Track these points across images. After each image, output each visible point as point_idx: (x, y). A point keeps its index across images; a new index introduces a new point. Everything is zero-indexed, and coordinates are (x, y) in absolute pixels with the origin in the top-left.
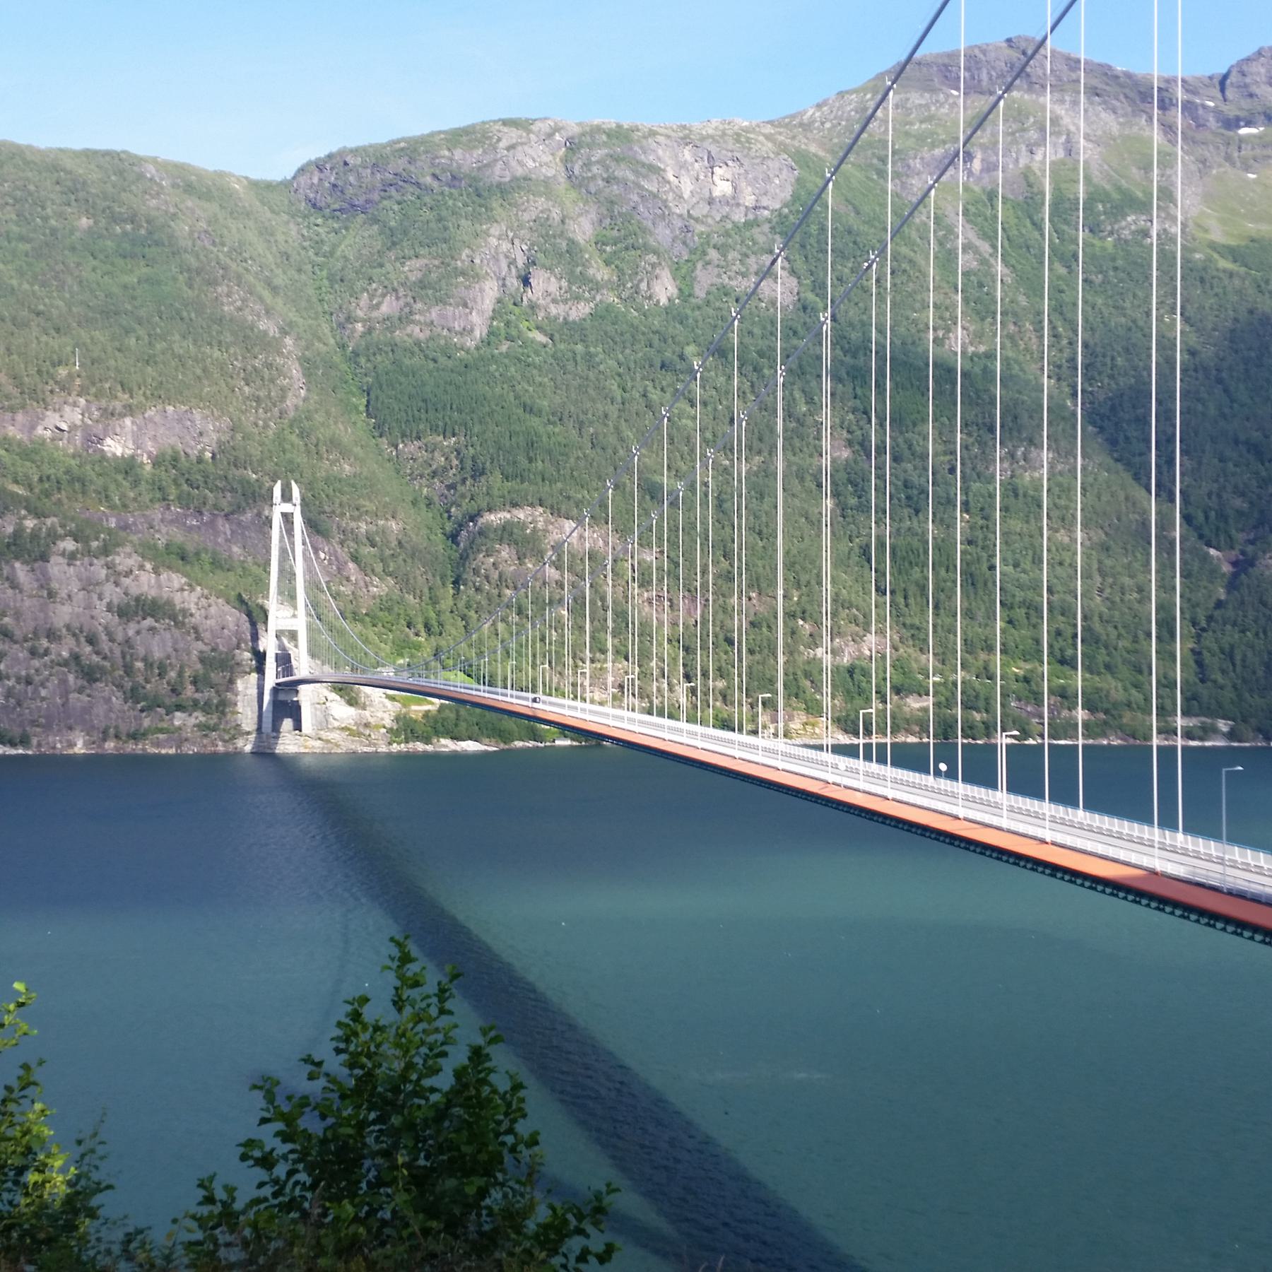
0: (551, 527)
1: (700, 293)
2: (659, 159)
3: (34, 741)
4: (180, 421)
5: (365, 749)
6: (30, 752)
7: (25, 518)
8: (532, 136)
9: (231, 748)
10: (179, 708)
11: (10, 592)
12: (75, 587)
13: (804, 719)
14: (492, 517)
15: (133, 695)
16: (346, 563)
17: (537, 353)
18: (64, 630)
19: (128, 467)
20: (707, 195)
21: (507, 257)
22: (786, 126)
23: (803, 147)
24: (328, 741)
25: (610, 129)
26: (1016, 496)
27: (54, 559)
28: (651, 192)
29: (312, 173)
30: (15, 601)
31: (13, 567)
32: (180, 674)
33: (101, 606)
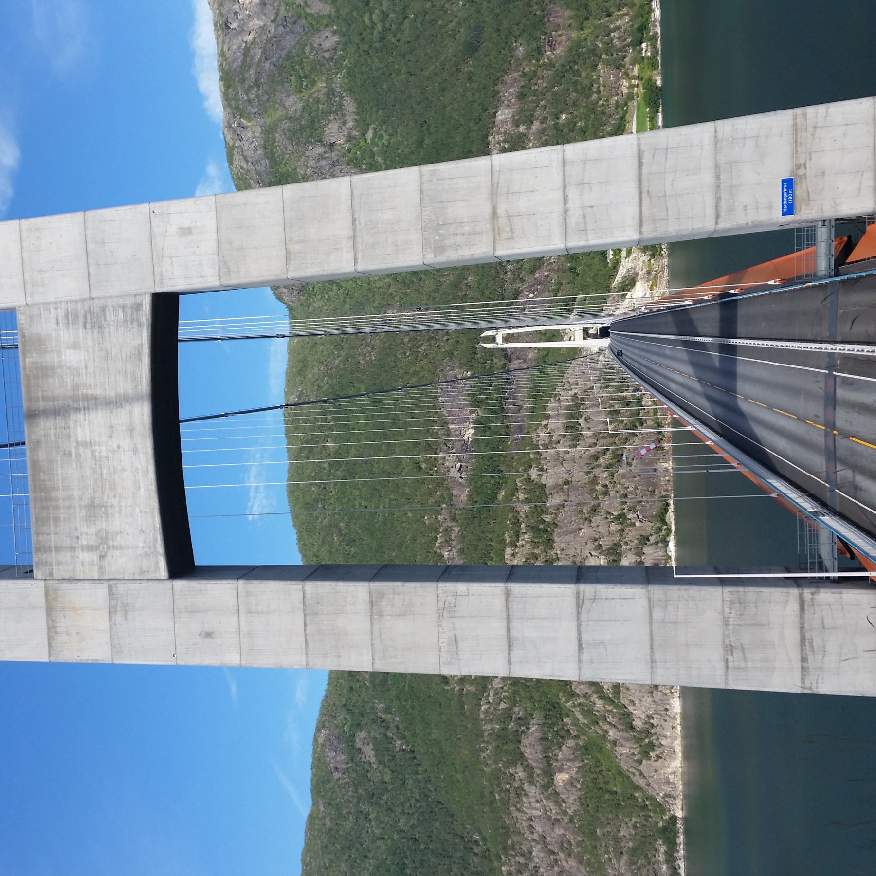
0: (502, 130)
2: (239, 48)
3: (664, 493)
5: (666, 274)
7: (518, 498)
8: (236, 145)
16: (535, 279)
17: (381, 137)
19: (481, 426)
20: (109, 424)
21: (318, 160)
25: (224, 85)
27: (543, 480)
28: (263, 53)
29: (281, 293)
31: (551, 507)
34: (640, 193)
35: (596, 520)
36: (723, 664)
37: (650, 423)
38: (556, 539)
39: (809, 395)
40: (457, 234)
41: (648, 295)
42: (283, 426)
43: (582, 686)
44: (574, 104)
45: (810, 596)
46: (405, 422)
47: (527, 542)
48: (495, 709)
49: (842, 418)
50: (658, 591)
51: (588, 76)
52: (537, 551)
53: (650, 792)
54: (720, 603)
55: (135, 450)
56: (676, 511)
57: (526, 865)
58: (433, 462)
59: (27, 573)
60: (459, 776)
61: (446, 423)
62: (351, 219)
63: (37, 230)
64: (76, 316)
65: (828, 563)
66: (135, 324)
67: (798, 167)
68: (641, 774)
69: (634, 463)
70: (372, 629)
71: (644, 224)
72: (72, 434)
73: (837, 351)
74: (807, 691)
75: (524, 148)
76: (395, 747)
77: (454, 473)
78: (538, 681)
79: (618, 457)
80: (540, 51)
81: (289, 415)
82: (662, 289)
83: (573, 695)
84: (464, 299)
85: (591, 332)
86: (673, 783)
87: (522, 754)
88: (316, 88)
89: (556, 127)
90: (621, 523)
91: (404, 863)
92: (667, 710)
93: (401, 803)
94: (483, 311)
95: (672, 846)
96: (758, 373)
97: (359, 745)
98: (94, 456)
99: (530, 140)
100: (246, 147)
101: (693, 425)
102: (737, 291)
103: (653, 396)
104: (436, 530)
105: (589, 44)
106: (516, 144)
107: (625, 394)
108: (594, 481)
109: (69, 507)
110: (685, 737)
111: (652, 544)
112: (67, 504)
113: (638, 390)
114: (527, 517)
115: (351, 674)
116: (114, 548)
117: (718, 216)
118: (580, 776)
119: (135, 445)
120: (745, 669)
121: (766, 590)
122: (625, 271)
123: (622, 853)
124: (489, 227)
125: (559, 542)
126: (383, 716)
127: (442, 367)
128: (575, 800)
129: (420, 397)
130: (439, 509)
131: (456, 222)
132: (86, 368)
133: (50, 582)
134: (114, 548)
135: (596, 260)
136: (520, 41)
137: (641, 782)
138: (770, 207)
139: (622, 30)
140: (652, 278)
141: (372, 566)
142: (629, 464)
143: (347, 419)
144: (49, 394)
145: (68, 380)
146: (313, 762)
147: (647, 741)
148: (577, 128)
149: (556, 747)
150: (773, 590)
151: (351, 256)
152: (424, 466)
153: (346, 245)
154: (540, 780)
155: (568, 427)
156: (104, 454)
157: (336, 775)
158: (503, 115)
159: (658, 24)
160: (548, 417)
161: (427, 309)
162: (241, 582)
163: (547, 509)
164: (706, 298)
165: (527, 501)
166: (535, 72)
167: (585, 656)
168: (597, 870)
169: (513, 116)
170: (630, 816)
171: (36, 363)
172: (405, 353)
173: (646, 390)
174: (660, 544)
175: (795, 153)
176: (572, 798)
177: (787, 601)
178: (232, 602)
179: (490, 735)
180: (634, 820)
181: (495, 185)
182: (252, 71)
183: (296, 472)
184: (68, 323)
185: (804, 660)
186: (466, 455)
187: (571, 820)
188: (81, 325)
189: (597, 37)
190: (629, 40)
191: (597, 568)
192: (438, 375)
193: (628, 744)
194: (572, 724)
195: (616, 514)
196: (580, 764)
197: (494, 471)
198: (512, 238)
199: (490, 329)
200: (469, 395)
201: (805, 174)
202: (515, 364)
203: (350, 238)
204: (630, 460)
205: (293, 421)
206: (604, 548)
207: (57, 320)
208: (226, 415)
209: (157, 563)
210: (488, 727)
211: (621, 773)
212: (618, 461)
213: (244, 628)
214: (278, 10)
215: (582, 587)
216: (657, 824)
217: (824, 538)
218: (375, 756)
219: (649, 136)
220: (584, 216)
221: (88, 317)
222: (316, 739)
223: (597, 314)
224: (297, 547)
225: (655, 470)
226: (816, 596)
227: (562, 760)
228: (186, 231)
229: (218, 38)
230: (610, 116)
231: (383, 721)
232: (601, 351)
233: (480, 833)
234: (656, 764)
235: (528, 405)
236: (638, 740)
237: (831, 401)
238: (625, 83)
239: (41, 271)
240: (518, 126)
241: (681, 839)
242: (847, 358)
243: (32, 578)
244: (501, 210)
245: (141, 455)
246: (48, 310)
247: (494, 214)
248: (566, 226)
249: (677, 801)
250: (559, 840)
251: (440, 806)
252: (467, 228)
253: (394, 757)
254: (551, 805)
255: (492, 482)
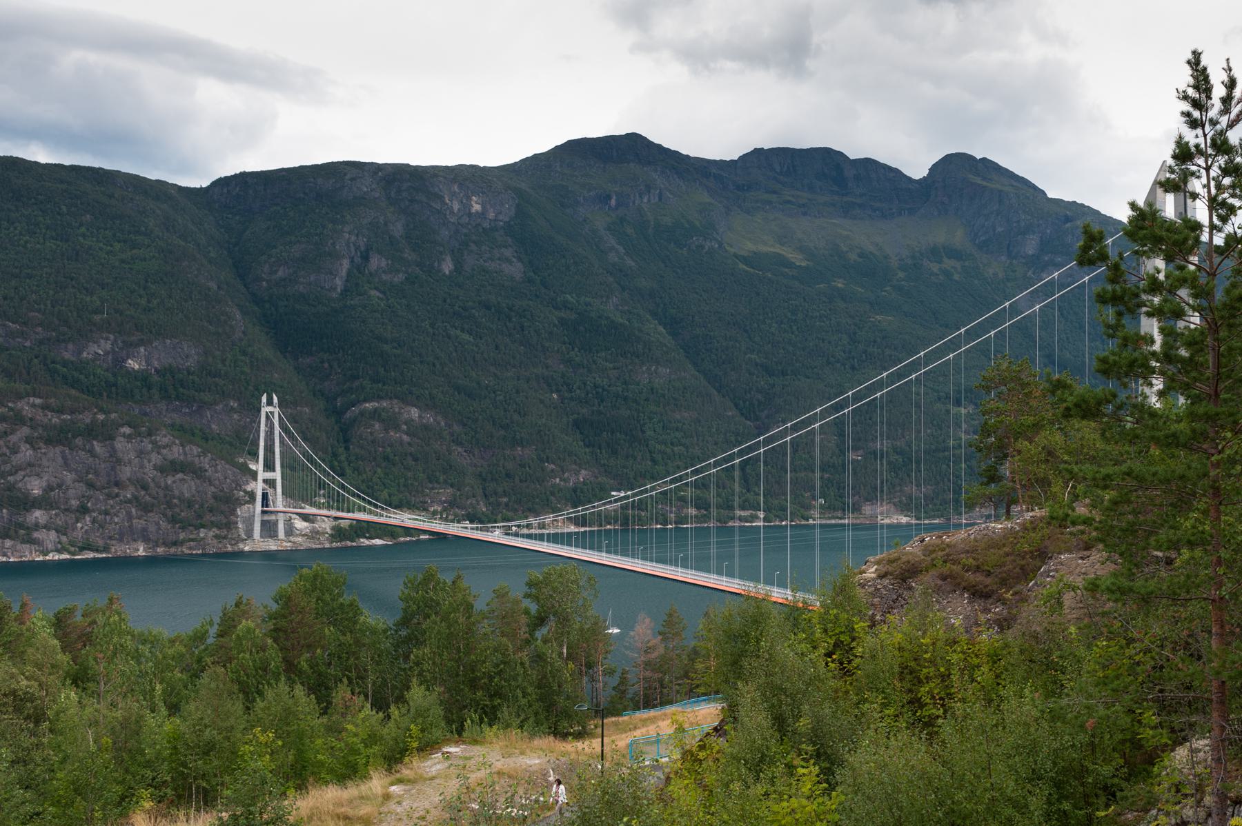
2: (440, 191)
4: (174, 348)
5: (317, 546)
6: (110, 556)
8: (366, 173)
9: (236, 548)
10: (203, 526)
12: (132, 455)
14: (367, 405)
15: (173, 520)
19: (143, 378)
24: (294, 543)
26: (653, 393)
30: (95, 464)
31: (93, 445)
32: (202, 506)
33: (149, 467)
35: (82, 487)
47: (50, 420)
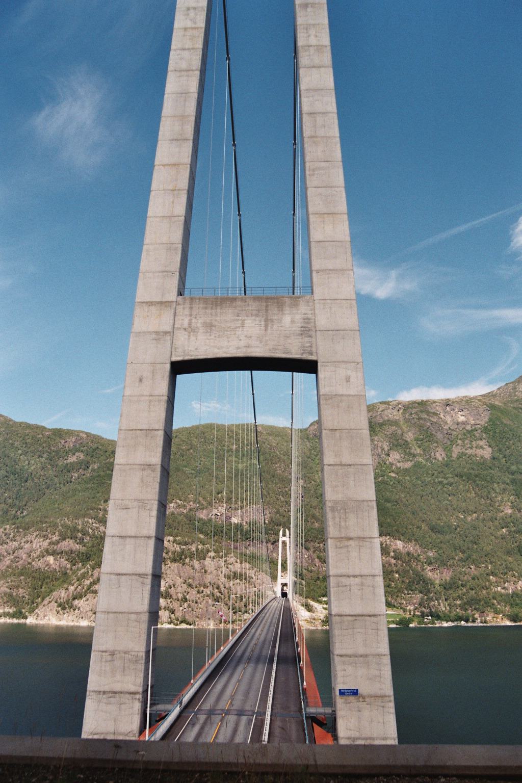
0: (392, 544)
1: (455, 455)
3: (196, 623)
5: (313, 628)
8: (390, 407)
11: (192, 570)
12: (213, 568)
13: (493, 615)
18: (209, 584)
19: (238, 527)
22: (487, 396)
23: (493, 403)
27: (207, 559)
28: (434, 422)
31: (193, 562)
34: (355, 616)
35: (185, 586)
36: (104, 649)
37: (235, 617)
38: (176, 564)
39: (245, 701)
40: (340, 518)
41: (303, 618)
42: (245, 422)
43: (97, 574)
44: (403, 581)
45: (138, 698)
46: (243, 487)
47: (176, 549)
48: (89, 527)
49: (232, 718)
50: (145, 618)
51: (416, 589)
52: (170, 554)
53: (41, 606)
54: (137, 650)
55: (238, 348)
56: (187, 629)
57: (9, 538)
58: (221, 501)
59: (180, 294)
60: (56, 506)
61: (242, 508)
62: (351, 463)
63: (351, 307)
64: (308, 323)
65: (154, 708)
66: (302, 352)
67: (364, 698)
68: (50, 602)
69: (214, 608)
70: (136, 464)
71: (339, 618)
72: (249, 318)
73: (266, 717)
74: (87, 693)
75: (382, 554)
76: (74, 473)
77: (215, 511)
78: (102, 551)
79: (217, 600)
80: (430, 564)
81: (251, 426)
82: (305, 626)
83: (93, 569)
84: (306, 521)
85: (285, 588)
86: (44, 618)
87: (65, 539)
88: (417, 448)
89: (392, 571)
90: (182, 600)
91: (15, 474)
92: (82, 618)
93: (46, 475)
94: (299, 530)
95: (13, 616)
96: (258, 675)
97: (77, 454)
98: (236, 327)
99: (386, 558)
100: (389, 411)
101: (232, 640)
102: (301, 665)
103: (249, 619)
104: (184, 501)
105: (432, 589)
106: (385, 550)
107: (251, 604)
108: (206, 586)
109: (211, 315)
110: (67, 627)
111: (170, 615)
112: (214, 314)
113: (252, 611)
114: (189, 549)
115: (113, 452)
116: (189, 336)
117: (341, 656)
118: (52, 569)
119: (241, 348)
120: (101, 661)
121: (142, 675)
122: (316, 606)
123: (11, 589)
124: (343, 535)
125: (175, 566)
126: (90, 468)
127: (271, 508)
128: (39, 566)
129: (256, 495)
130: (196, 503)
131: (346, 518)
132: (282, 326)
133: (175, 304)
134: (189, 336)
135: (322, 591)
136: (436, 554)
137: (45, 602)
138: (344, 683)
139: (438, 607)
140: (311, 621)
141: (169, 466)
142: (213, 606)
143: (247, 456)
144: (269, 308)
145: (276, 317)
146: (70, 430)
147: (67, 606)
148: (391, 583)
149: (67, 558)
150: (142, 679)
151: (332, 463)
152: (220, 496)
153: (337, 461)
154: (51, 548)
155: (235, 573)
156: (237, 333)
157: (63, 442)
158: (400, 544)
159: (440, 625)
160: (241, 563)
161: (302, 501)
162: (166, 398)
163: (192, 560)
164: (299, 649)
165: (197, 549)
166: (420, 561)
167: (113, 577)
168: (4, 575)
169: (399, 549)
170: (29, 595)
171: (285, 303)
172: (280, 489)
173: (252, 616)
174: (169, 620)
175: (370, 696)
176: (40, 565)
177: (136, 685)
178: (156, 393)
179: (76, 523)
180: (27, 597)
181: (364, 540)
182: (426, 416)
183: (220, 428)
184: (304, 319)
185: (104, 693)
186: (224, 518)
187: (29, 563)
188: (303, 325)
189: (435, 593)
190: (433, 610)
191: (159, 586)
192: (267, 505)
193: (66, 596)
194: (78, 567)
195: (187, 597)
196: (57, 570)
197: (214, 532)
198: (336, 548)
199: (290, 534)
200: (256, 521)
201: (360, 701)
202: (270, 546)
203: (341, 462)
204: (215, 606)
205: (247, 428)
206: (170, 590)
207: (306, 314)
208: (253, 394)
209: (179, 356)
210: (80, 523)
211: (51, 591)
212: (215, 599)
213: (143, 398)
214: (455, 431)
215: (150, 577)
216: (24, 608)
217: (168, 707)
218: (71, 462)
219: (384, 620)
220: (346, 586)
221: (307, 329)
222: (83, 432)
223: (295, 592)
224: (182, 427)
225: (209, 619)
226: (137, 701)
227: (60, 560)
228: (348, 380)
229: (442, 400)
230: (396, 600)
231: (88, 467)
232: (275, 592)
233: (26, 515)
234: (55, 611)
235: (248, 552)
236: (67, 602)
237: (240, 713)
238: (412, 608)
239: (331, 308)
240: (393, 552)
241: (15, 621)
242: (262, 722)
243: (178, 295)
244: (351, 542)
245: (235, 351)
246: (311, 310)
247: (350, 539)
248: (341, 576)
249: (35, 620)
250: (20, 556)
251: (42, 495)
252: (343, 524)
253: (69, 472)
254: (38, 553)
255: (209, 532)
